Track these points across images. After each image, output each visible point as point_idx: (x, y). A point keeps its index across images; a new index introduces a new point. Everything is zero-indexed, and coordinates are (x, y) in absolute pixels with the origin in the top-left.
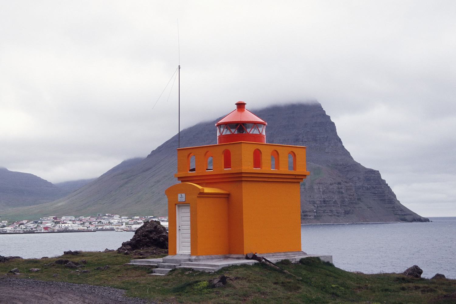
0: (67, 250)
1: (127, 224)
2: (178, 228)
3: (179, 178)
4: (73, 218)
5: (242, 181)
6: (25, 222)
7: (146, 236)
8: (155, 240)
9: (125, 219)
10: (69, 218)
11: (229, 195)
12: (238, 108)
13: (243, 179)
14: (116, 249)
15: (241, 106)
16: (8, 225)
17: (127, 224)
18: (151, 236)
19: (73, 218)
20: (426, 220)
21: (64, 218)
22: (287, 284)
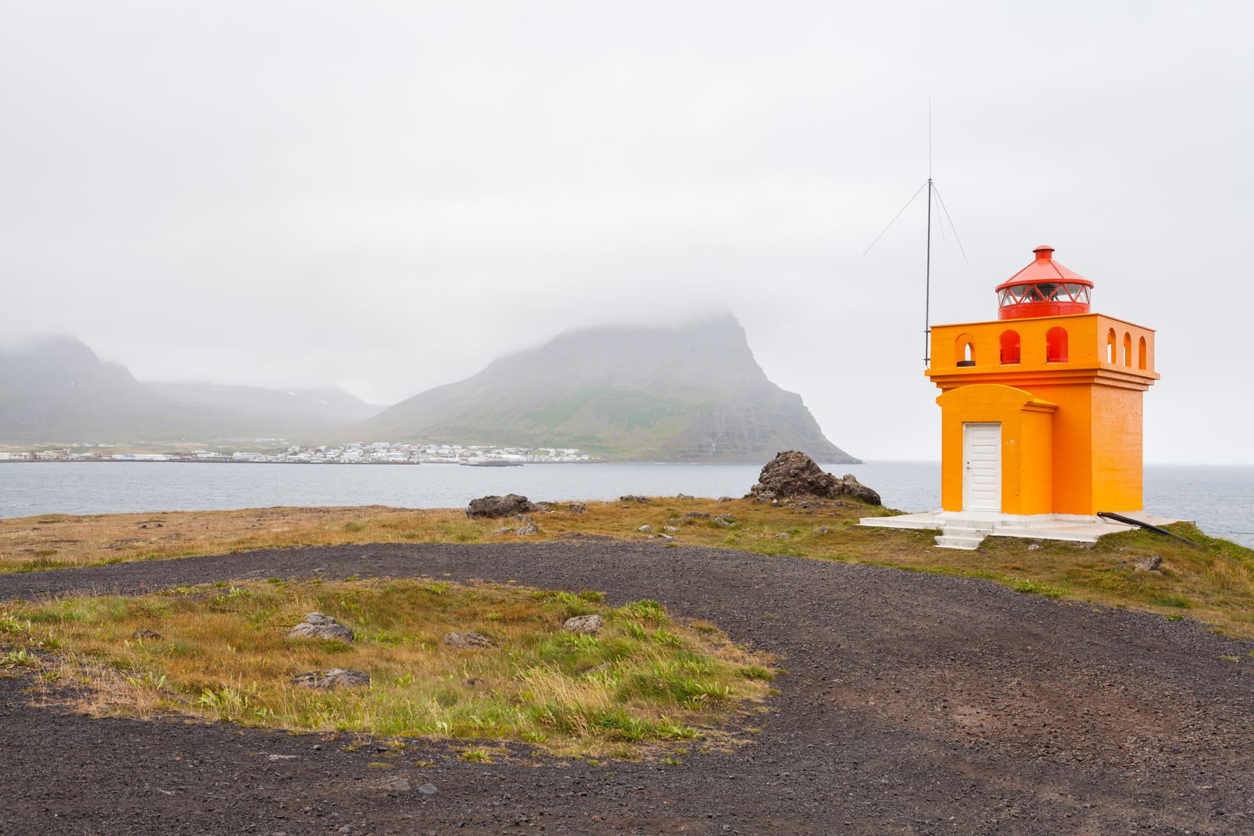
0: (625, 495)
1: (461, 455)
2: (965, 466)
3: (933, 378)
4: (388, 445)
5: (1090, 384)
6: (323, 448)
7: (796, 475)
8: (811, 483)
9: (458, 449)
10: (382, 444)
11: (1056, 408)
12: (1038, 258)
13: (1096, 381)
14: (740, 495)
15: (1043, 254)
16: (301, 452)
17: (461, 455)
18: (804, 476)
19: (388, 445)
20: (859, 462)
21: (376, 444)
22: (278, 596)
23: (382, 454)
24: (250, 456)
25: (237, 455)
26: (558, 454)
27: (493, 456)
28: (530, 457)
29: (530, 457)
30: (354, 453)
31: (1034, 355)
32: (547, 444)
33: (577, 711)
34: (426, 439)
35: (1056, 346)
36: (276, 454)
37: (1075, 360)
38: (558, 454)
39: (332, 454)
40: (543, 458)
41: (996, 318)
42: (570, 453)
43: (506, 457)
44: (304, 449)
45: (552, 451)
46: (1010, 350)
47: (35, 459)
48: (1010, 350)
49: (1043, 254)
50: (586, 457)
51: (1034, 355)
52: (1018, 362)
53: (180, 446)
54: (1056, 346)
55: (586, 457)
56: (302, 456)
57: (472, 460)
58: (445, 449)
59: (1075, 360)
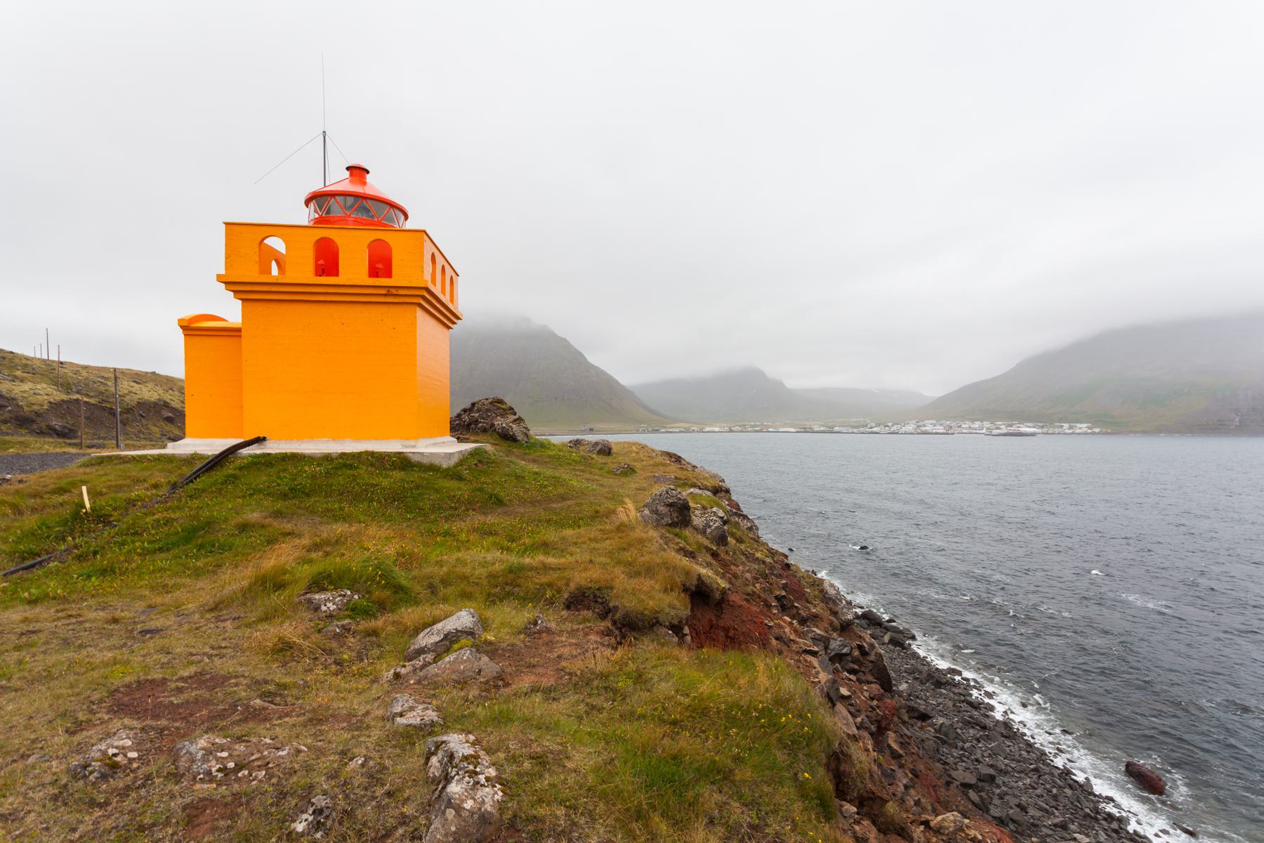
9: (987, 424)
23: (929, 428)
24: (844, 430)
25: (836, 429)
26: (1071, 428)
27: (1013, 429)
28: (1045, 430)
29: (1045, 430)
30: (910, 427)
31: (353, 269)
32: (1061, 420)
33: (980, 780)
34: (963, 418)
35: (380, 263)
36: (861, 428)
37: (399, 278)
38: (1071, 428)
39: (894, 428)
40: (1057, 431)
41: (306, 224)
42: (1083, 427)
43: (1024, 429)
44: (878, 425)
45: (1066, 426)
46: (327, 260)
47: (731, 431)
48: (327, 260)
49: (358, 172)
50: (1097, 430)
51: (353, 269)
52: (337, 274)
53: (807, 424)
54: (380, 263)
55: (1097, 430)
56: (875, 429)
57: (995, 432)
58: (977, 425)
59: (399, 278)
